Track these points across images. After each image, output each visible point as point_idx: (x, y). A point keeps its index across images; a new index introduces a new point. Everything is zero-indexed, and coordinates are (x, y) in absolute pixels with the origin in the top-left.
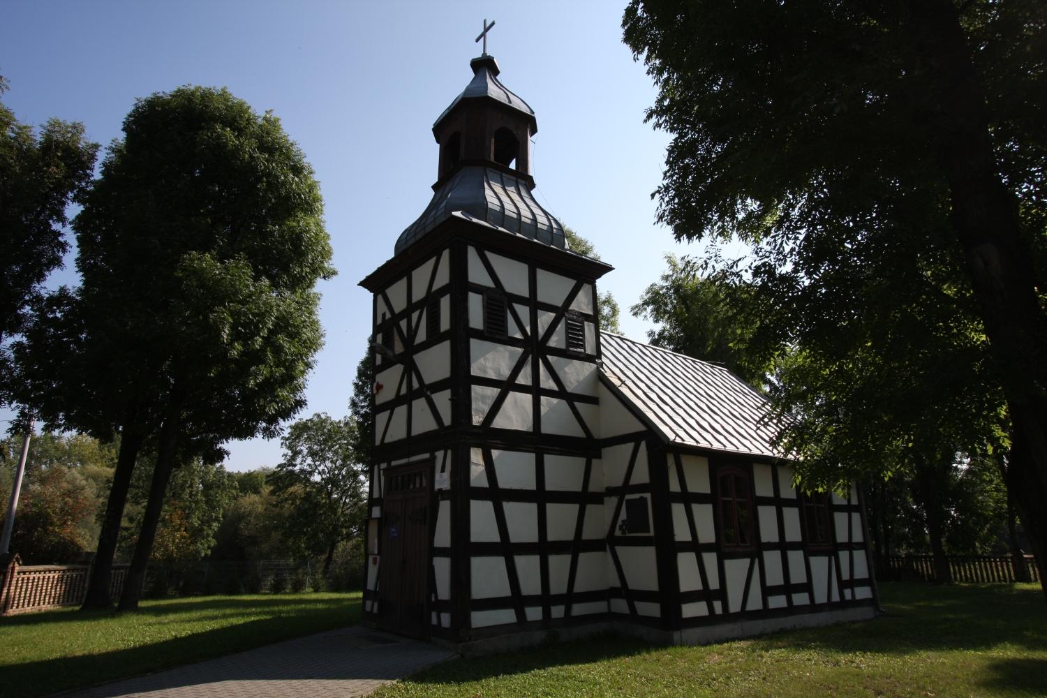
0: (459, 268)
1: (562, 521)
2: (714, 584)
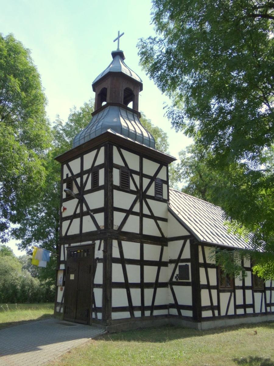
0: (109, 156)
1: (150, 274)
2: (215, 303)
